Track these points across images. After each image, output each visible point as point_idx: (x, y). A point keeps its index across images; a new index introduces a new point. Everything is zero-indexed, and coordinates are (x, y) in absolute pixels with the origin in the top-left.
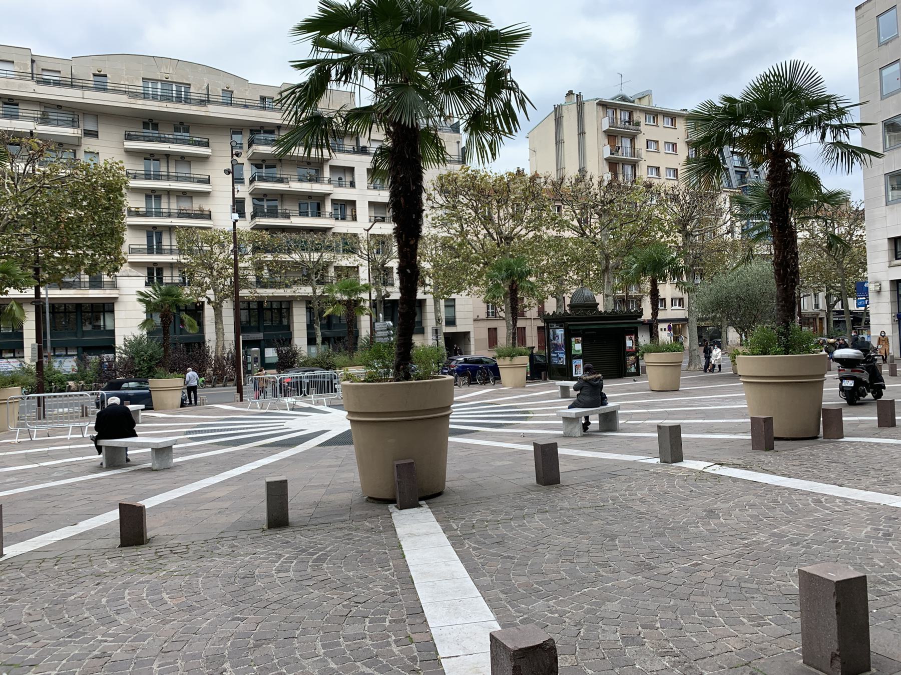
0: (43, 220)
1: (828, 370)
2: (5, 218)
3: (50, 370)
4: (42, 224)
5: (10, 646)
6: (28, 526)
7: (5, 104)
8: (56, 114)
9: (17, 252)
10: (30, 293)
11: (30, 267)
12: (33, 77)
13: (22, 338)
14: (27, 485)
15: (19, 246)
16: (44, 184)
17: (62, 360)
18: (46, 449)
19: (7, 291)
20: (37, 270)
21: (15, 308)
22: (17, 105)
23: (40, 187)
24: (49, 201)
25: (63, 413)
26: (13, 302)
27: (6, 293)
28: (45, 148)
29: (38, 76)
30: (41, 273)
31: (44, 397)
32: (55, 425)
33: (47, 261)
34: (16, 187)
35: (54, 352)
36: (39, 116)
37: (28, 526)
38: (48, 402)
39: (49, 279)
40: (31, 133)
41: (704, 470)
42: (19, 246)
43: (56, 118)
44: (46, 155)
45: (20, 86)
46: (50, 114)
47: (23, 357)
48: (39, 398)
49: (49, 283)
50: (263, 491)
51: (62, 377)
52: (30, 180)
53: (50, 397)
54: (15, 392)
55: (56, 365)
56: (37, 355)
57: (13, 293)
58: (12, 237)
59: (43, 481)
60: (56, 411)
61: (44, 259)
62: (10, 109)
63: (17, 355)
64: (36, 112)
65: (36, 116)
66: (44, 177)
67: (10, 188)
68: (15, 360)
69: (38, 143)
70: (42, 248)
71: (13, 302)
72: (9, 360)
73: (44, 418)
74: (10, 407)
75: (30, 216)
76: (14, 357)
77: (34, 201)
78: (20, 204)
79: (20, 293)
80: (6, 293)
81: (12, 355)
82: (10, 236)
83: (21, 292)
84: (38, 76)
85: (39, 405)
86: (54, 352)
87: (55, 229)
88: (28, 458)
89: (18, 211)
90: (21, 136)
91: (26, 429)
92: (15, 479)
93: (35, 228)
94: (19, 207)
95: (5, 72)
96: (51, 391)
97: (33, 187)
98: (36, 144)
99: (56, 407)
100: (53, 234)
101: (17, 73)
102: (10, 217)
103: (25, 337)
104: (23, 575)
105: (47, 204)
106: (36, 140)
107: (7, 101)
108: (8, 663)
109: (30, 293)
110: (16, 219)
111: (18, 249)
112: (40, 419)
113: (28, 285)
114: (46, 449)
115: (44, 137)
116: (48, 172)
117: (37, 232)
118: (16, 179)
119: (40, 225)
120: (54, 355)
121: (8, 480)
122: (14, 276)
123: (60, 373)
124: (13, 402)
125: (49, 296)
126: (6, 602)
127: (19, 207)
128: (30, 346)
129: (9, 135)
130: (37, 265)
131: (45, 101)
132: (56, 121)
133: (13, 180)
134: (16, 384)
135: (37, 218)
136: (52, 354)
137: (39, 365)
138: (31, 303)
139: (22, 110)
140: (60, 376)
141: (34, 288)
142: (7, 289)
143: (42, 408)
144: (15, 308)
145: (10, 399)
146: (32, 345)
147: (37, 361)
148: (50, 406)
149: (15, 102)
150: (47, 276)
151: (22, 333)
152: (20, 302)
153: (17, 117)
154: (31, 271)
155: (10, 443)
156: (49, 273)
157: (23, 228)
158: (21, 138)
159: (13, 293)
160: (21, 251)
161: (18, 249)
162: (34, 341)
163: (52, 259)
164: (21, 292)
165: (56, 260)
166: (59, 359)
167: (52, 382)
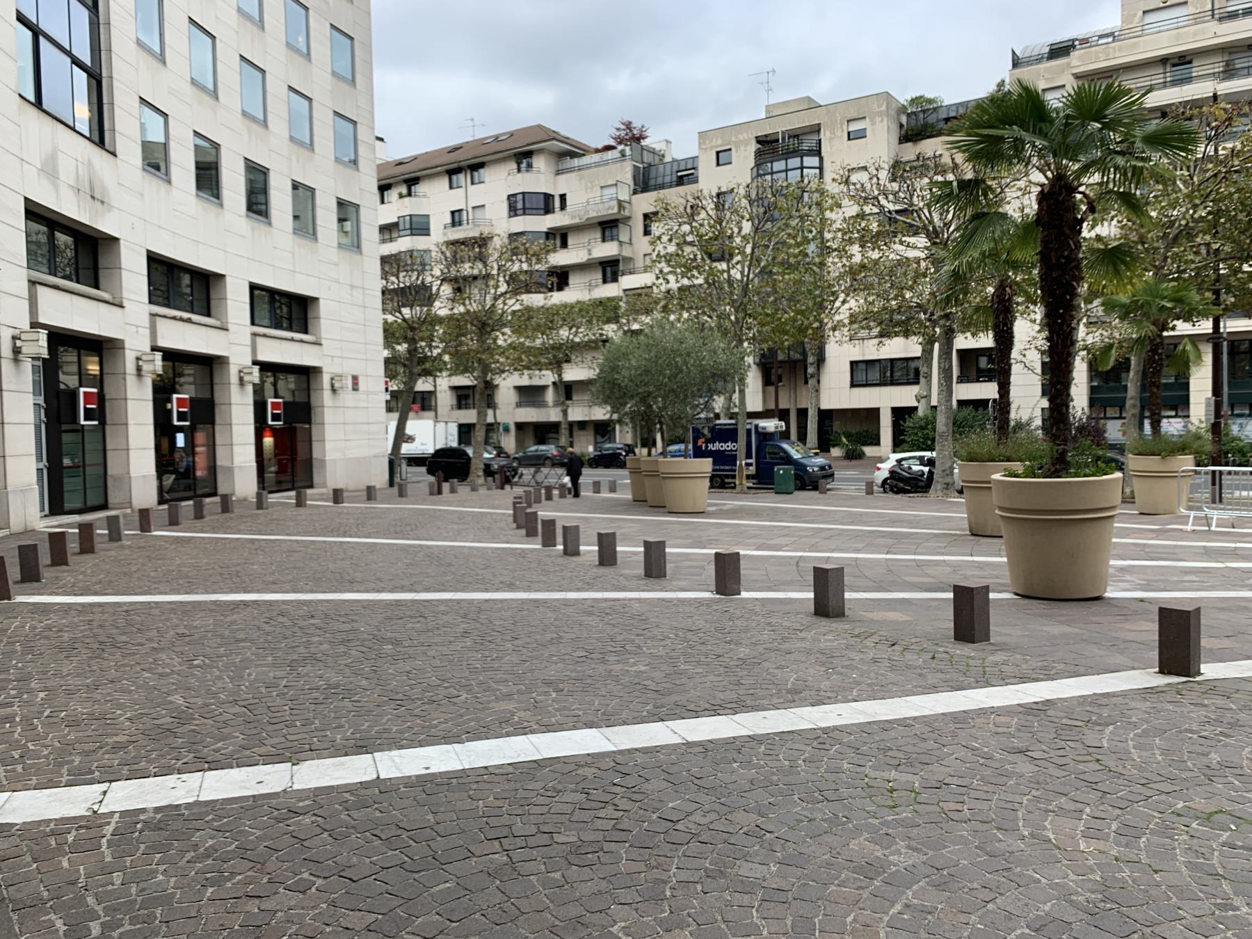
0: (1229, 219)
1: (535, 502)
2: (1177, 225)
3: (1227, 435)
4: (1228, 226)
5: (1233, 794)
6: (1226, 643)
7: (1174, 65)
8: (1246, 59)
9: (1191, 270)
10: (1206, 326)
11: (1208, 290)
12: (1213, 16)
13: (1187, 389)
14: (1213, 588)
15: (1193, 262)
16: (1232, 167)
17: (1245, 422)
18: (1233, 545)
19: (1175, 326)
20: (1217, 293)
21: (1189, 347)
22: (1190, 62)
23: (1226, 172)
24: (1239, 190)
25: (1240, 498)
26: (1186, 339)
27: (1173, 328)
28: (1235, 113)
29: (1221, 11)
30: (1223, 297)
31: (1221, 472)
32: (1244, 514)
33: (1233, 279)
34: (1192, 179)
35: (1232, 410)
36: (1221, 69)
37: (1226, 643)
38: (1226, 480)
39: (1234, 304)
40: (1215, 97)
41: (104, 787)
42: (1193, 262)
43: (1246, 65)
44: (1236, 124)
45: (1195, 34)
46: (1237, 61)
47: (1189, 416)
48: (1214, 472)
49: (1231, 311)
50: (17, 552)
51: (1244, 447)
52: (1210, 166)
53: (1229, 473)
54: (1186, 463)
55: (1235, 429)
56: (1213, 413)
57: (1182, 328)
58: (1185, 251)
59: (1234, 587)
60: (1237, 494)
61: (1229, 276)
62: (1181, 71)
63: (1180, 413)
64: (1217, 65)
65: (1216, 70)
66: (1232, 156)
67: (1184, 182)
68: (1180, 420)
69: (1224, 109)
70: (1224, 260)
71: (1186, 339)
72: (1171, 420)
73: (1221, 501)
74: (1183, 481)
75: (1210, 217)
76: (1176, 416)
77: (1218, 194)
78: (1197, 202)
79: (1191, 327)
80: (1173, 328)
81: (1173, 413)
82: (1182, 249)
83: (1194, 325)
84: (1221, 11)
85: (1214, 484)
86: (1232, 410)
87: (1246, 230)
88: (1208, 554)
89: (1195, 212)
90: (1200, 104)
91: (1201, 514)
92: (1196, 579)
93: (1217, 232)
94: (1195, 207)
95: (1176, 20)
96: (1227, 465)
97: (1215, 175)
98: (1222, 112)
99: (1237, 488)
100: (1243, 237)
101: (1191, 17)
102: (1183, 222)
103: (1192, 388)
104: (1234, 707)
105: (1236, 196)
106: (1223, 105)
107: (1176, 61)
108: (1233, 813)
109: (1206, 326)
110: (1191, 224)
111: (1193, 266)
112: (1214, 502)
113: (1204, 315)
114: (1233, 545)
115: (1233, 98)
116: (1239, 147)
117: (1219, 239)
118: (1192, 169)
119: (1225, 228)
120: (1232, 415)
121: (1186, 578)
122: (1189, 304)
123: (1240, 440)
124: (1185, 475)
125: (1228, 330)
126: (1216, 735)
127: (1195, 207)
128: (1204, 401)
129: (1185, 108)
130: (1217, 286)
131: (1229, 45)
132: (1246, 70)
133: (1188, 171)
134: (1187, 451)
135: (1220, 218)
136: (1230, 413)
137: (1216, 428)
138: (1208, 341)
139: (1197, 69)
140: (1241, 444)
141: (1211, 319)
142: (1175, 322)
143: (1217, 487)
144: (1189, 347)
145: (1183, 471)
146: (1208, 399)
147: (1212, 421)
148: (1229, 487)
149: (1188, 59)
150: (1233, 300)
151: (1188, 384)
152: (1195, 339)
153: (1188, 80)
154: (1209, 295)
155: (1181, 530)
156: (1235, 296)
157: (1201, 235)
158: (1201, 107)
159: (1182, 328)
160: (1197, 268)
161: (1193, 266)
162: (1210, 394)
163: (1240, 275)
164: (1194, 325)
165: (1246, 276)
166: (1239, 421)
167: (1228, 453)
